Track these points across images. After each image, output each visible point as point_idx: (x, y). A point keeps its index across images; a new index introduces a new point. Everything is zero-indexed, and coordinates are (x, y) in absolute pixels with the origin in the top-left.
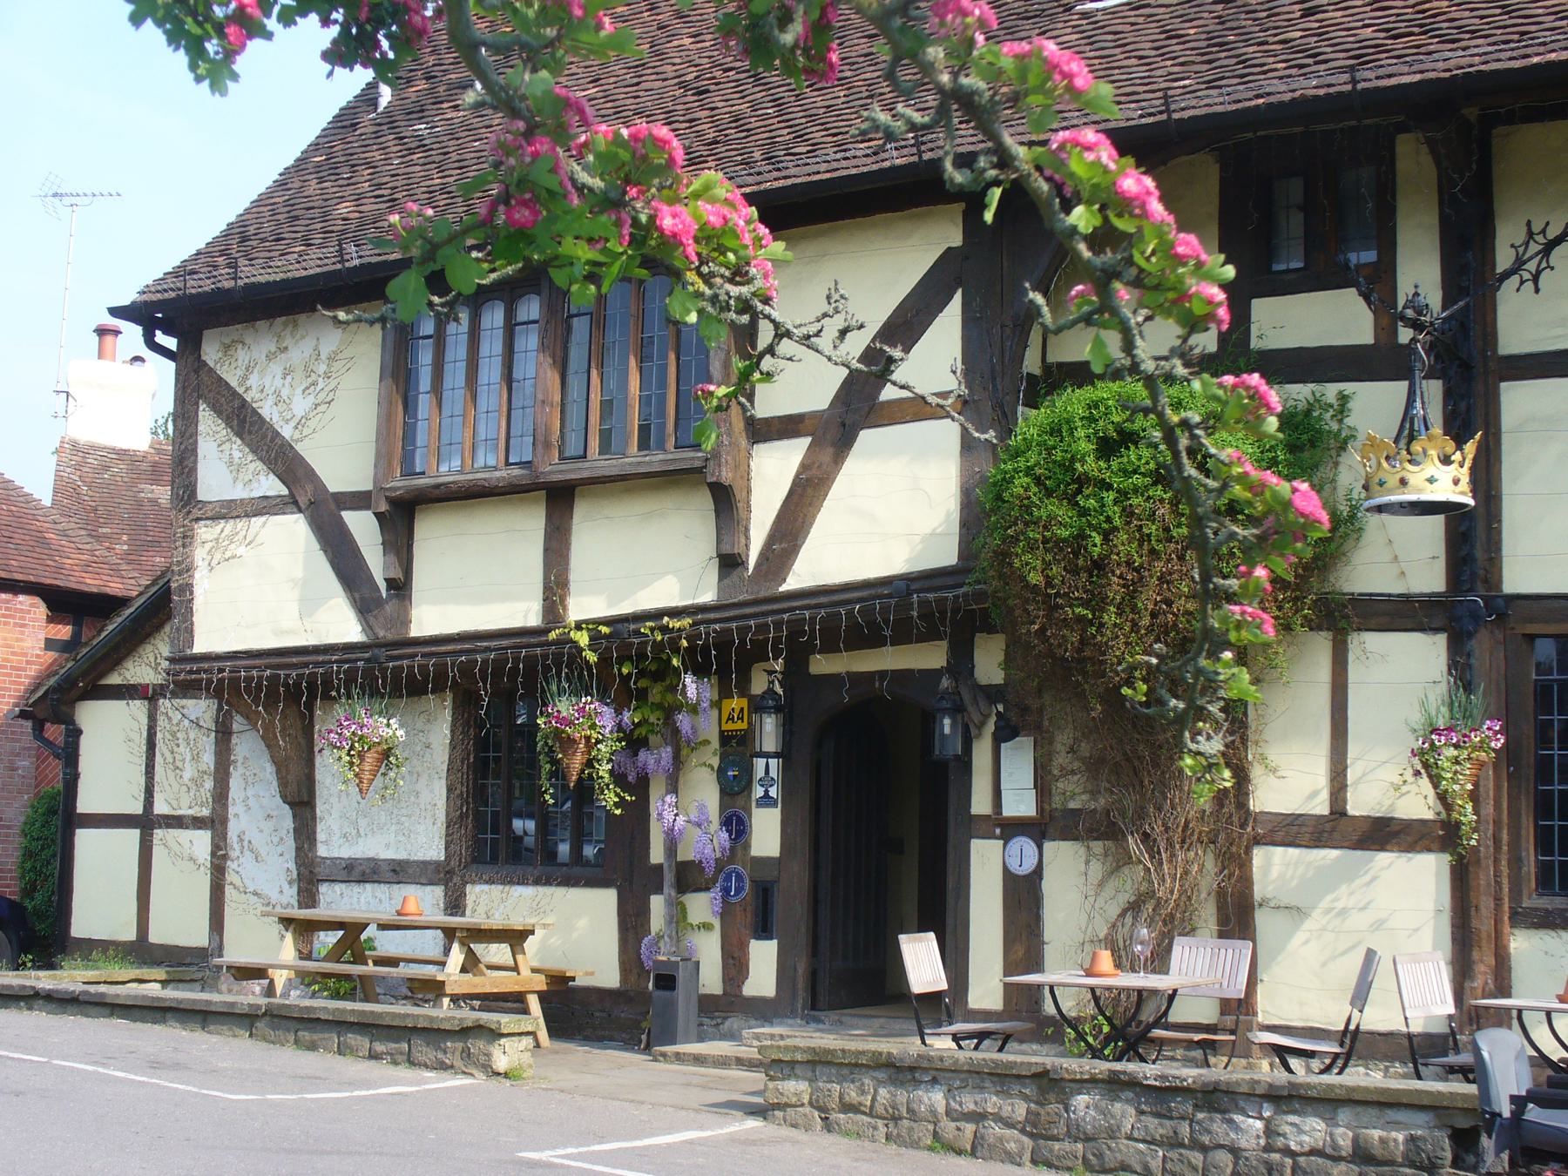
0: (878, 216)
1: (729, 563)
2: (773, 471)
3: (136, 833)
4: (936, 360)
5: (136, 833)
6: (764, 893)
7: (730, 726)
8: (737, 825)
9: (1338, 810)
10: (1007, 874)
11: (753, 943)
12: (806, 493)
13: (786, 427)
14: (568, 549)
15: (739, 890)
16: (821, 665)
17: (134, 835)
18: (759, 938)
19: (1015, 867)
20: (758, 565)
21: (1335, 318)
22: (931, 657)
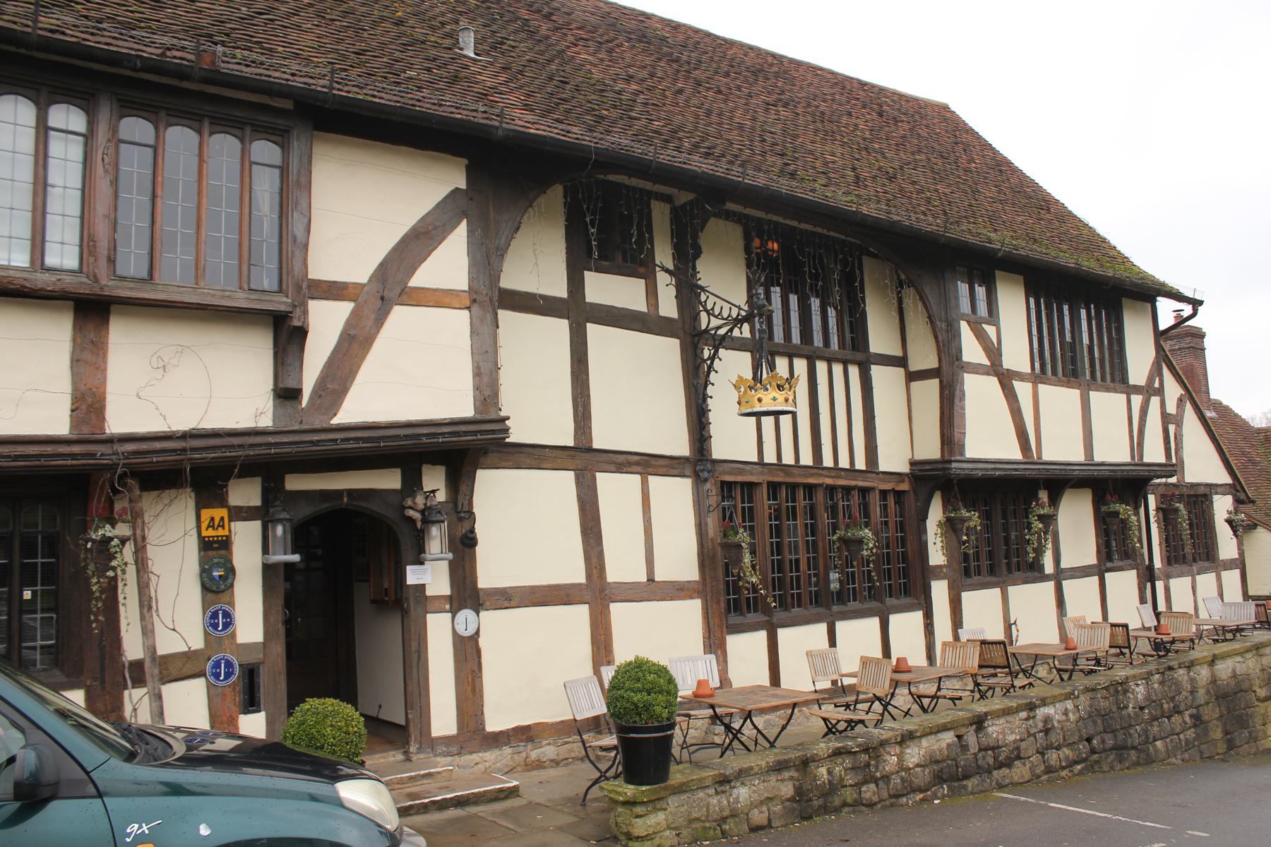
0: (404, 148)
1: (286, 394)
2: (326, 323)
3: (579, 577)
4: (449, 264)
5: (579, 577)
6: (251, 673)
7: (211, 532)
8: (219, 620)
9: (651, 579)
10: (456, 636)
11: (241, 716)
12: (354, 344)
13: (334, 291)
14: (105, 362)
15: (228, 675)
16: (295, 483)
17: (575, 573)
18: (245, 713)
19: (461, 630)
20: (311, 398)
21: (622, 291)
22: (390, 480)
